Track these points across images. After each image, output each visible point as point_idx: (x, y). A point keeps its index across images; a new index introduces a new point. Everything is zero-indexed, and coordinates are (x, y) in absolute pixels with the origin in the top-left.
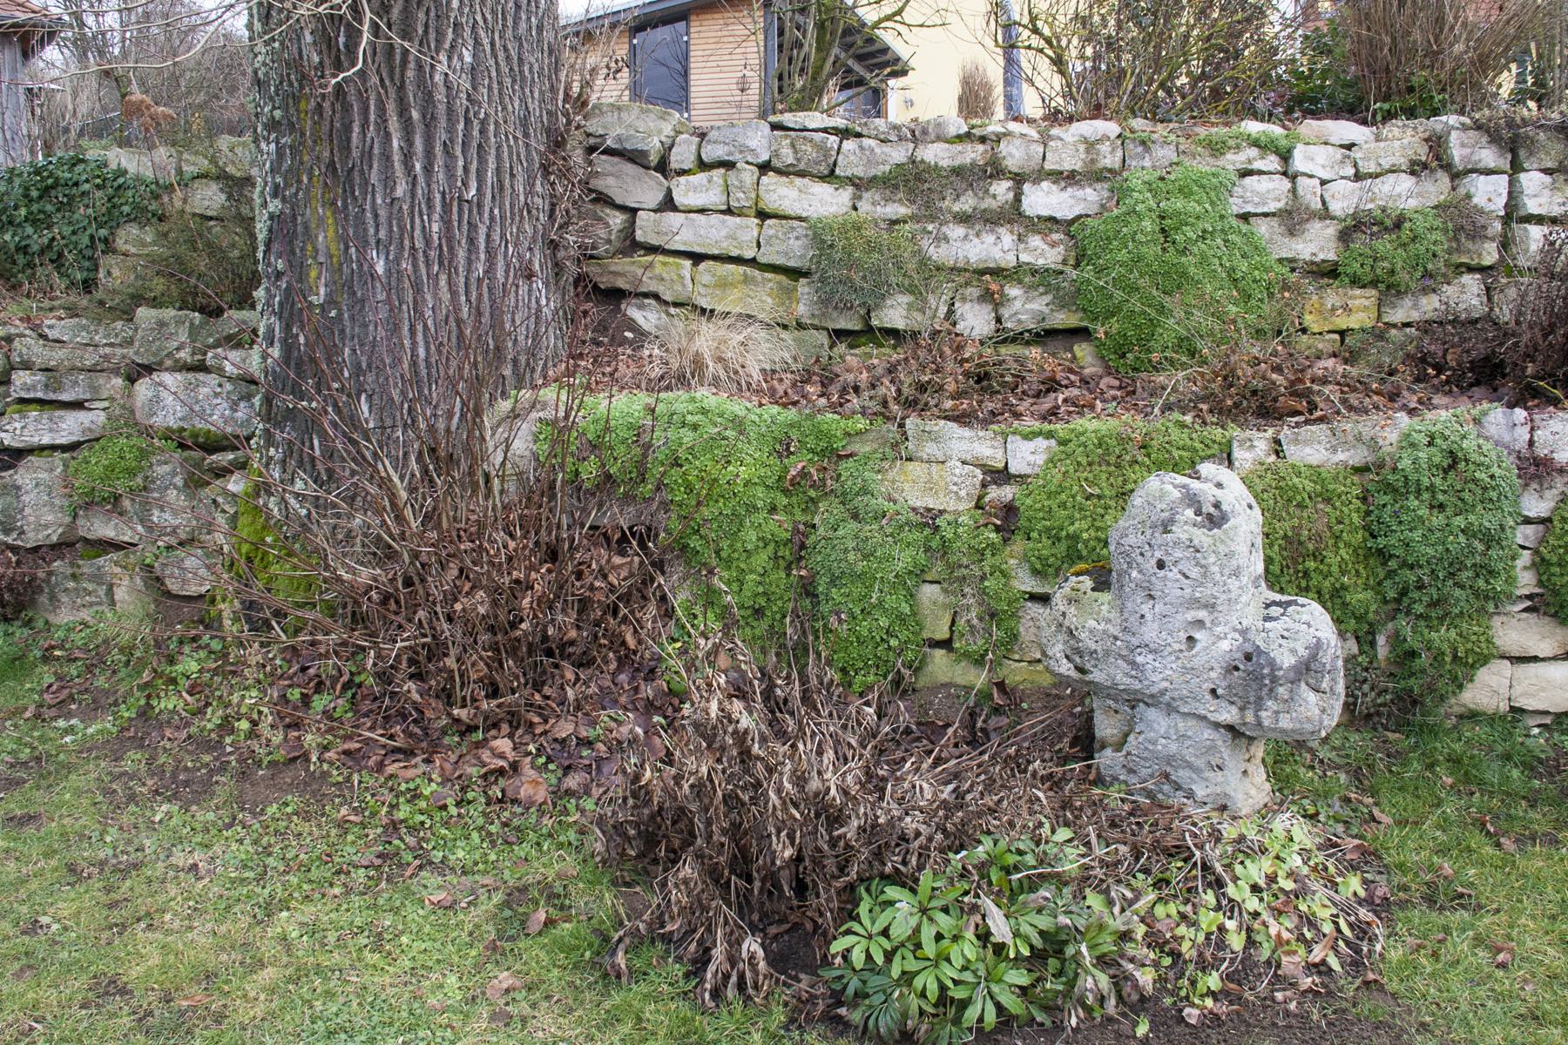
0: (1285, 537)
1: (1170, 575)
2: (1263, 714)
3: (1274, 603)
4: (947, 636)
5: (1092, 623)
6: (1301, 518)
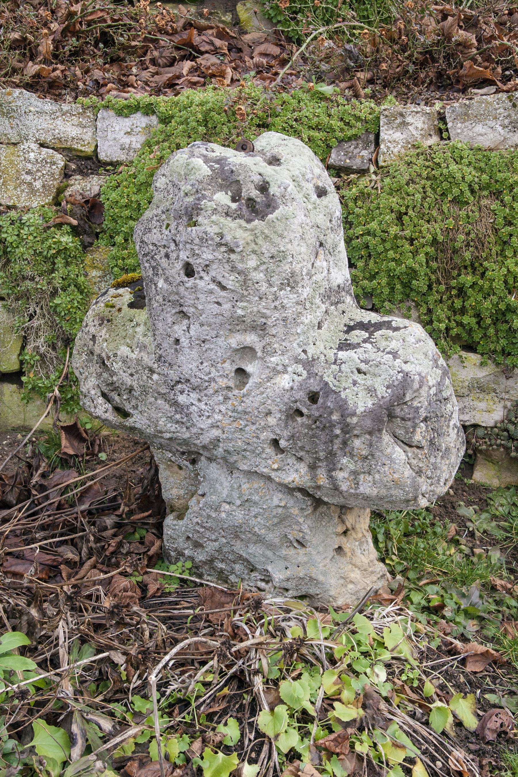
0: (435, 242)
1: (201, 284)
2: (340, 475)
3: (362, 326)
4: (15, 366)
5: (124, 350)
6: (456, 219)
